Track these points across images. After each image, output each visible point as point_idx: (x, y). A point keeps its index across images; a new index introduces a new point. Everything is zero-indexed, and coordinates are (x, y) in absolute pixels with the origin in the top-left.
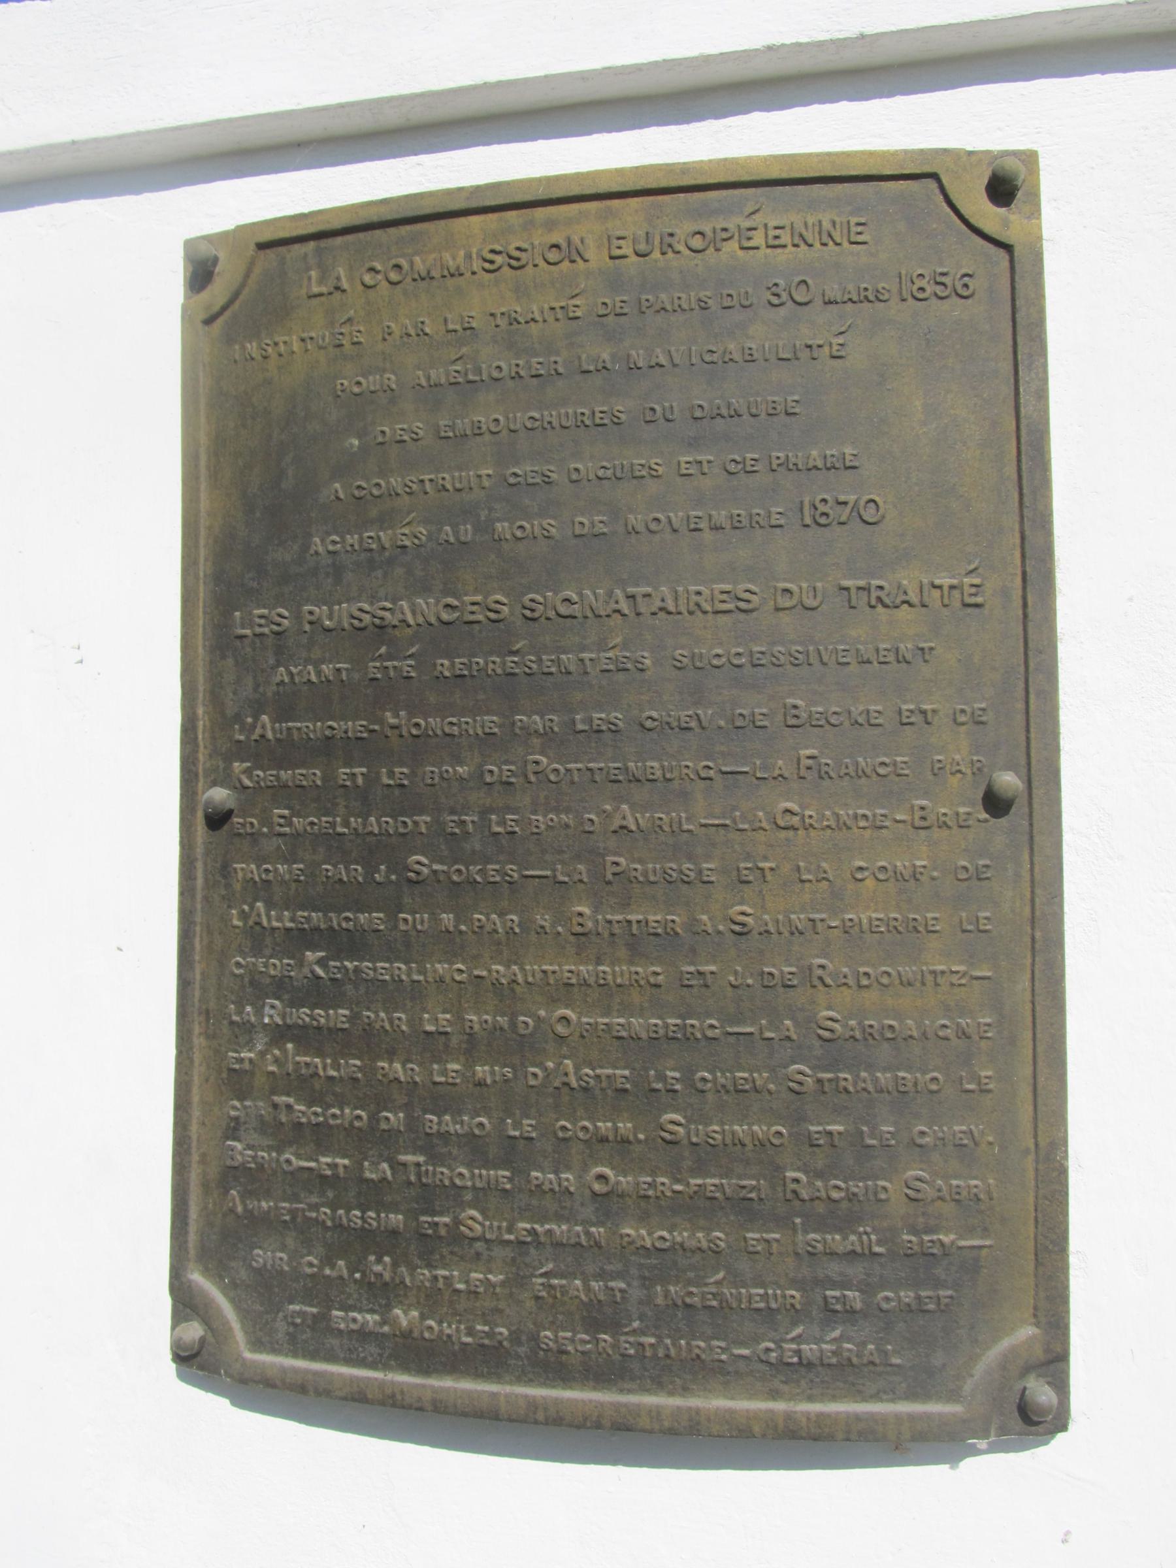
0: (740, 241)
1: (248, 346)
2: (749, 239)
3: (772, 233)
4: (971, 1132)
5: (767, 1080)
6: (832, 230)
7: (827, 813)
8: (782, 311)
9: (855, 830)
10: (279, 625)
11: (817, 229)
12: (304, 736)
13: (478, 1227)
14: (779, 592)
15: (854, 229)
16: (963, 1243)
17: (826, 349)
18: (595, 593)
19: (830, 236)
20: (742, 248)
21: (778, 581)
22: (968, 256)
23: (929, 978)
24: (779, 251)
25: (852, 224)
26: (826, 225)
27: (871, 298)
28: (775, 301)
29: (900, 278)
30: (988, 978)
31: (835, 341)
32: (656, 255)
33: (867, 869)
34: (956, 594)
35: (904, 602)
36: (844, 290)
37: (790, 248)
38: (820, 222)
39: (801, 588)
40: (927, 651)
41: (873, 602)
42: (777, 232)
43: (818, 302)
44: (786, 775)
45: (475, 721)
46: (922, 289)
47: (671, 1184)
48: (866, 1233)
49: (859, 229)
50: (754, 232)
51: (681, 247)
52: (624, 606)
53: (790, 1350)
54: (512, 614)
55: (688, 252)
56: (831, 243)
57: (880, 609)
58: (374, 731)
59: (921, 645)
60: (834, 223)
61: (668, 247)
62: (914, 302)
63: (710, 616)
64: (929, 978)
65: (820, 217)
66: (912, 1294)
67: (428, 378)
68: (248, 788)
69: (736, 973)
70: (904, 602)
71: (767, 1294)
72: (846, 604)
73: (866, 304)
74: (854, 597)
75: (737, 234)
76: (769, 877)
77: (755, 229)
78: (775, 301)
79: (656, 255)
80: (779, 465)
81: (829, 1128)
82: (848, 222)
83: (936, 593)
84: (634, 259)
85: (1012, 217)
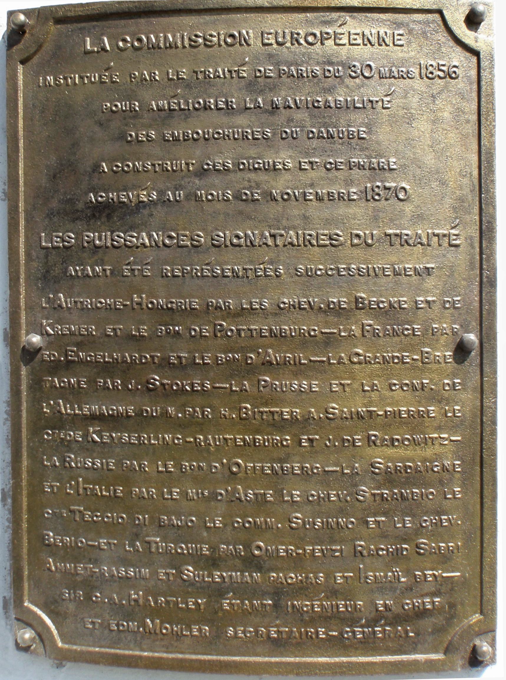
0: (335, 40)
1: (48, 78)
2: (340, 39)
3: (352, 37)
4: (309, 302)
5: (347, 495)
6: (385, 37)
7: (378, 355)
8: (357, 80)
9: (392, 364)
10: (68, 242)
11: (377, 35)
12: (85, 306)
13: (191, 574)
14: (353, 236)
15: (396, 37)
16: (445, 575)
17: (380, 103)
18: (253, 233)
19: (384, 41)
20: (336, 44)
21: (353, 229)
22: (457, 58)
23: (430, 441)
24: (356, 47)
25: (395, 35)
26: (382, 33)
27: (405, 76)
28: (353, 74)
29: (420, 66)
30: (459, 441)
31: (385, 99)
32: (288, 45)
33: (398, 384)
34: (446, 239)
35: (419, 243)
36: (391, 71)
37: (362, 46)
38: (378, 32)
39: (365, 234)
40: (374, 102)
41: (403, 243)
42: (355, 37)
43: (376, 76)
44: (356, 334)
45: (185, 302)
46: (431, 73)
47: (296, 549)
48: (397, 571)
49: (399, 37)
50: (342, 36)
51: (302, 41)
52: (270, 242)
53: (358, 631)
54: (205, 241)
55: (306, 45)
56: (384, 44)
57: (406, 246)
58: (126, 305)
59: (371, 99)
60: (386, 33)
61: (295, 40)
62: (427, 80)
63: (316, 249)
64: (430, 441)
65: (378, 29)
66: (252, 465)
67: (157, 106)
68: (51, 335)
69: (329, 440)
70: (419, 243)
71: (346, 604)
72: (389, 243)
73: (402, 80)
74: (393, 239)
75: (333, 36)
76: (347, 389)
77: (343, 34)
78: (353, 74)
79: (288, 45)
80: (354, 166)
81: (272, 409)
82: (394, 33)
83: (436, 239)
84: (275, 46)
85: (479, 36)
